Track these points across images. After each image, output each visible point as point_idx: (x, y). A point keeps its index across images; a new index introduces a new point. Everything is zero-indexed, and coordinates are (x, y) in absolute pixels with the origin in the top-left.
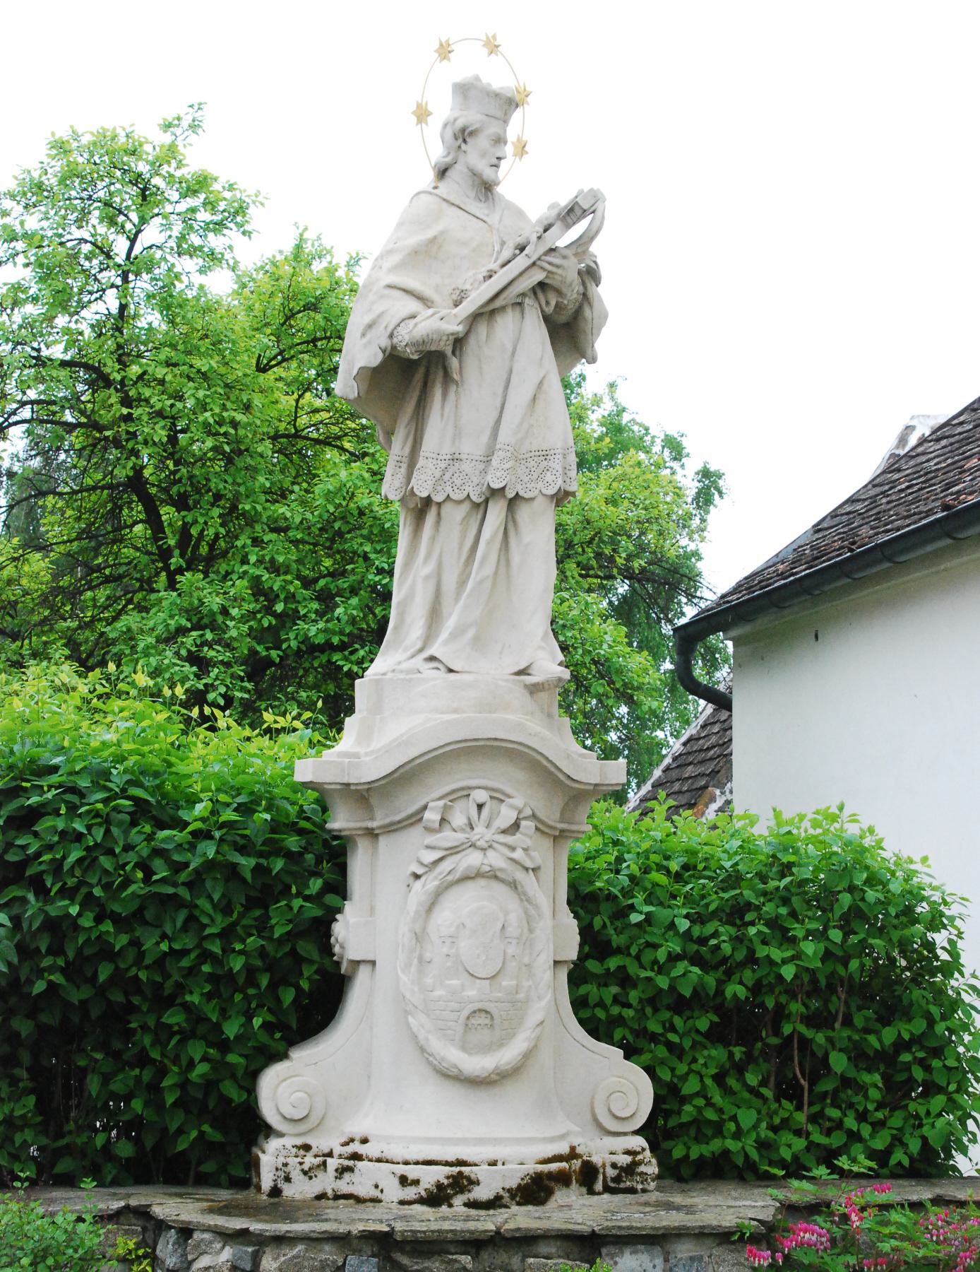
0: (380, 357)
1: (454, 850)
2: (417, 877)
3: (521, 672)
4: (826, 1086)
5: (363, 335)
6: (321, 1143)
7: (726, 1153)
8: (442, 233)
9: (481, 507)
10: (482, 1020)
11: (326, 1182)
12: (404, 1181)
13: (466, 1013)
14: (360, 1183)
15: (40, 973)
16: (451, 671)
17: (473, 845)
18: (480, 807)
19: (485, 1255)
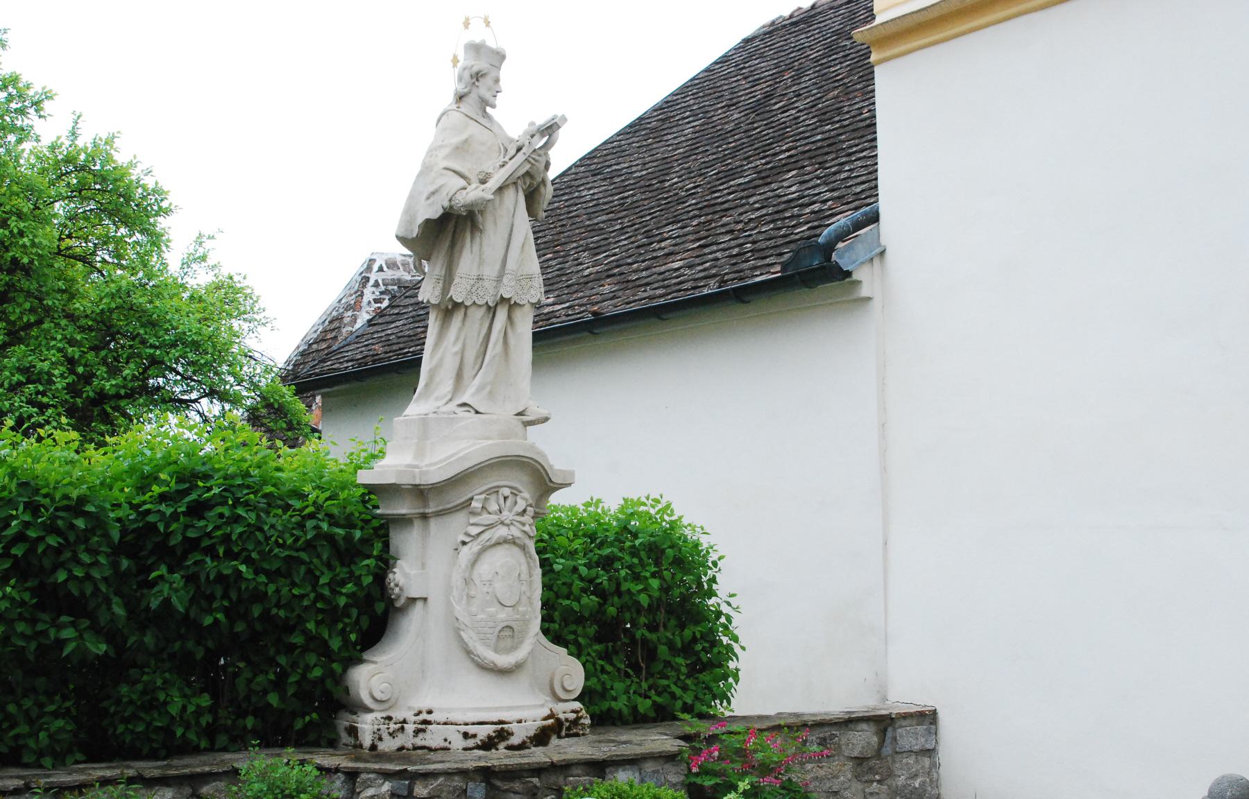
0: (441, 211)
1: (490, 526)
2: (464, 543)
3: (520, 414)
4: (659, 667)
5: (428, 198)
6: (398, 715)
7: (610, 709)
8: (471, 136)
9: (492, 310)
10: (507, 633)
11: (407, 739)
12: (466, 735)
13: (499, 628)
14: (433, 738)
15: (210, 611)
16: (477, 412)
17: (502, 523)
18: (505, 498)
19: (543, 777)
